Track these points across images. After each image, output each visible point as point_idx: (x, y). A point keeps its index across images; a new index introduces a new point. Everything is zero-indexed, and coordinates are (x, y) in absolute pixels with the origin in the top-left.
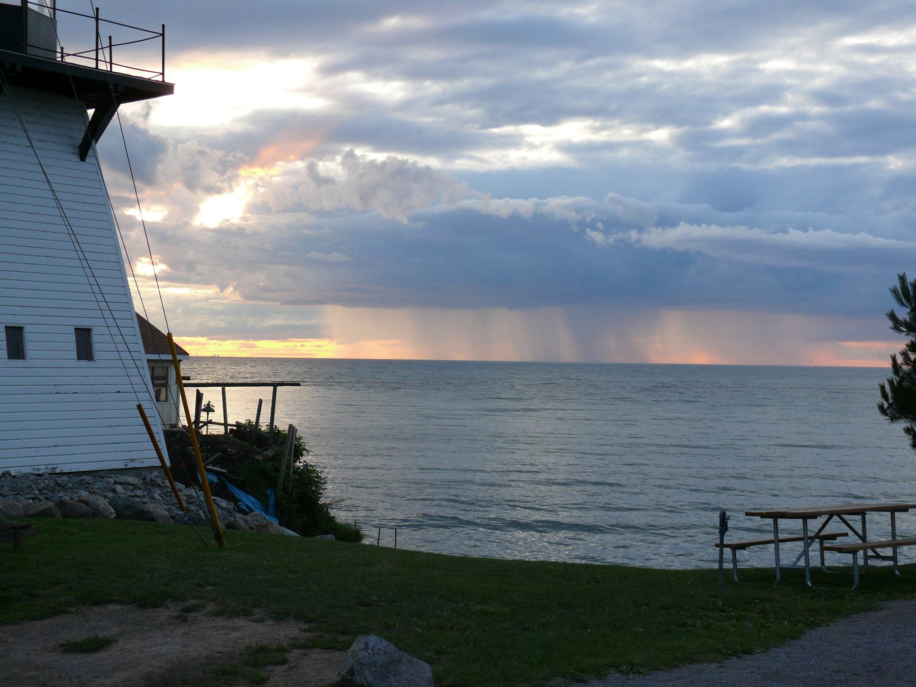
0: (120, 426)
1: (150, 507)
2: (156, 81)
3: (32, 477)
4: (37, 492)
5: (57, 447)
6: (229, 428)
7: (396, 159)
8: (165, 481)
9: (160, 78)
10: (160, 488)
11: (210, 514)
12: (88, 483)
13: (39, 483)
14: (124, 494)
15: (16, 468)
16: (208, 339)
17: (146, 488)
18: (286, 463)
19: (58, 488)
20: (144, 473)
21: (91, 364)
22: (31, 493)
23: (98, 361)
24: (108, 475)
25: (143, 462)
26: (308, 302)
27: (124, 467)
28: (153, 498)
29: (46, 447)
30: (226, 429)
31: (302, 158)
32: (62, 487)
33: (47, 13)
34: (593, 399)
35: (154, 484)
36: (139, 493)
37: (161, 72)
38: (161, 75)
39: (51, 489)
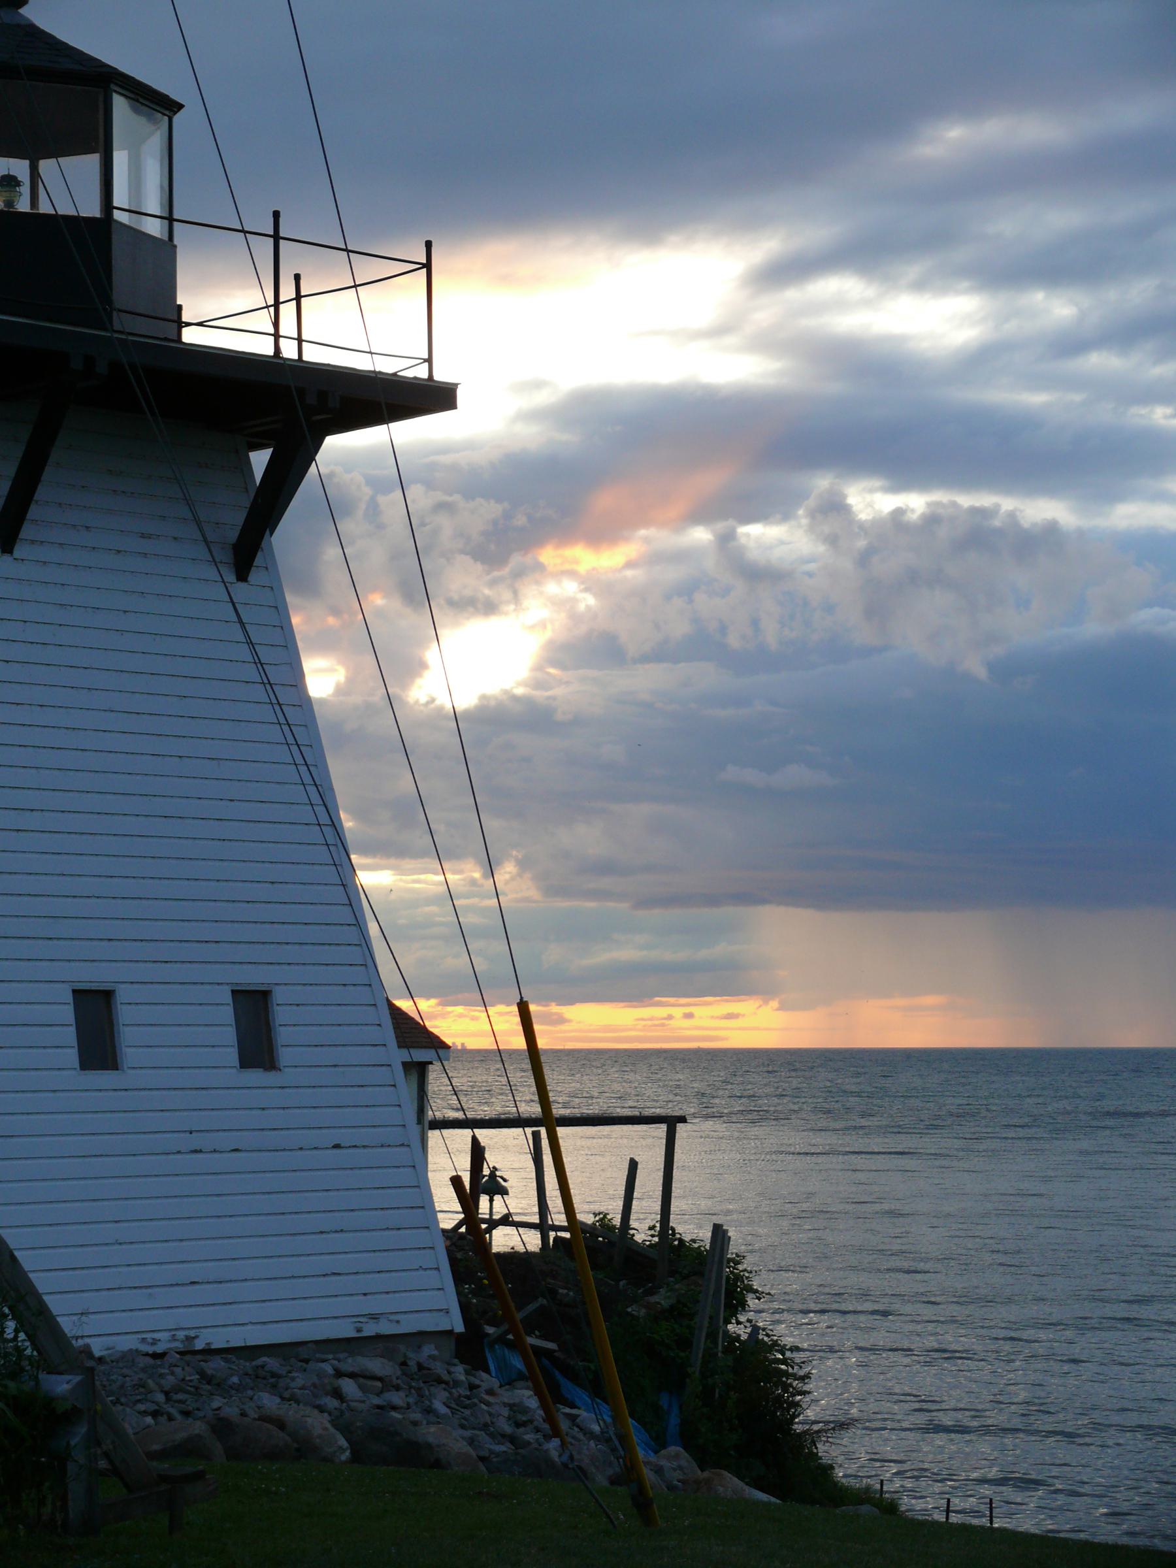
0: (342, 1231)
1: (430, 1433)
2: (415, 378)
3: (143, 1362)
4: (161, 1398)
5: (197, 1287)
6: (552, 1234)
7: (954, 504)
8: (452, 1369)
9: (422, 372)
10: (444, 1386)
11: (620, 1443)
12: (274, 1375)
13: (161, 1376)
14: (363, 1402)
15: (104, 1338)
16: (439, 1004)
17: (411, 1387)
18: (706, 1323)
19: (208, 1387)
20: (402, 1348)
21: (270, 1078)
22: (147, 1400)
23: (286, 1070)
24: (317, 1356)
25: (398, 1322)
26: (712, 900)
27: (354, 1334)
28: (429, 1411)
29: (172, 1285)
30: (545, 1238)
31: (699, 516)
32: (218, 1385)
33: (154, 228)
34: (1136, 1142)
35: (426, 1377)
36: (397, 1398)
37: (426, 356)
38: (427, 364)
39: (192, 1389)
